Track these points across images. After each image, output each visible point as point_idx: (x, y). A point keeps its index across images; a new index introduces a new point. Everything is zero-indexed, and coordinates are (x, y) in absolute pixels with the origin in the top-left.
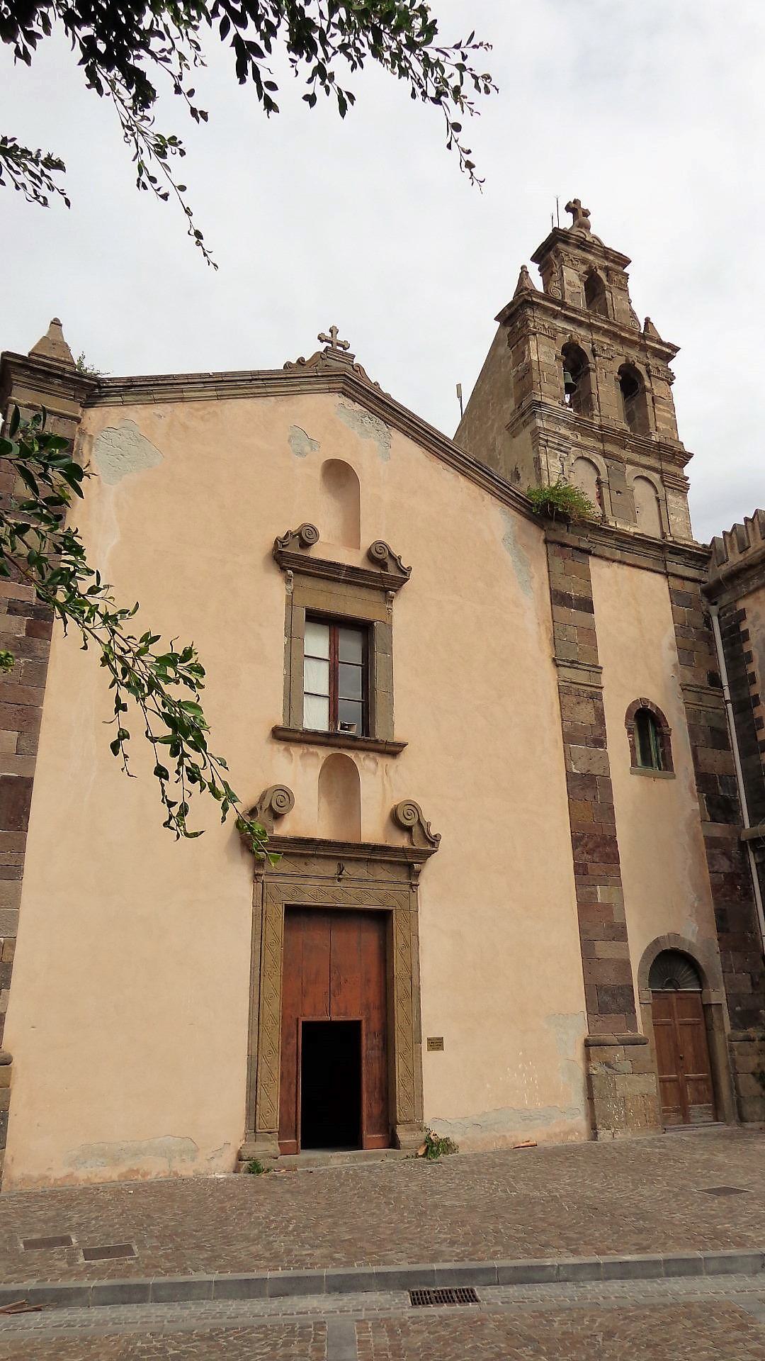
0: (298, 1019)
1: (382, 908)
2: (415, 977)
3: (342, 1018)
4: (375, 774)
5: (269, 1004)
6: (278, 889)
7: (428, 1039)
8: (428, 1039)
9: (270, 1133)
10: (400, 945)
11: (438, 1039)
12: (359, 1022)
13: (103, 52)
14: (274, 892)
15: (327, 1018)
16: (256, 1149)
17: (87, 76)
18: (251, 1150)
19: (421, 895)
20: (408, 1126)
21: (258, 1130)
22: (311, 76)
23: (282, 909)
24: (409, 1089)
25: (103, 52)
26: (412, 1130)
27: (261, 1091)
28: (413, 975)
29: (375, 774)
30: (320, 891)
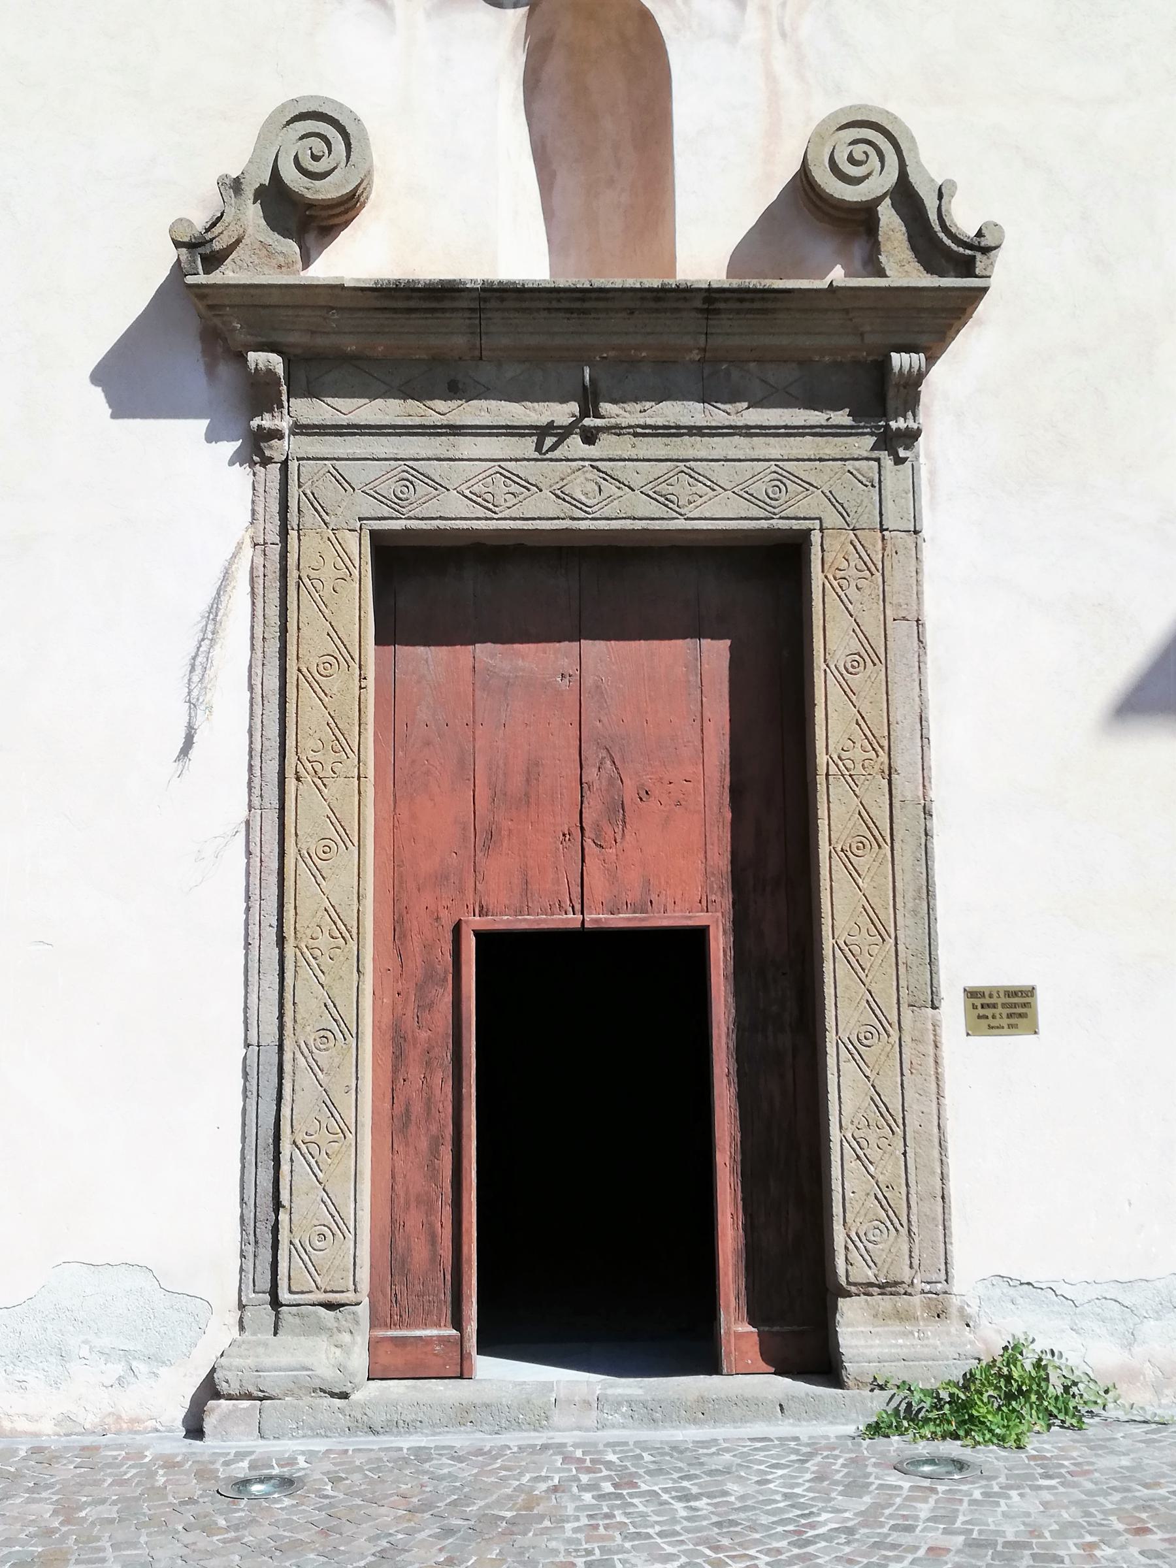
0: (457, 930)
1: (764, 524)
2: (906, 760)
3: (622, 920)
4: (733, 39)
5: (319, 875)
6: (342, 481)
7: (972, 994)
8: (972, 994)
9: (330, 1306)
10: (840, 657)
11: (1012, 993)
12: (697, 937)
13: (208, 421)
14: (328, 492)
15: (569, 920)
16: (267, 1362)
17: (206, 434)
18: (250, 1362)
19: (932, 473)
20: (885, 1303)
21: (284, 1296)
22: (241, 1145)
23: (359, 551)
24: (888, 1169)
25: (208, 421)
26: (902, 1316)
27: (295, 1171)
28: (899, 762)
29: (733, 39)
30: (510, 476)
